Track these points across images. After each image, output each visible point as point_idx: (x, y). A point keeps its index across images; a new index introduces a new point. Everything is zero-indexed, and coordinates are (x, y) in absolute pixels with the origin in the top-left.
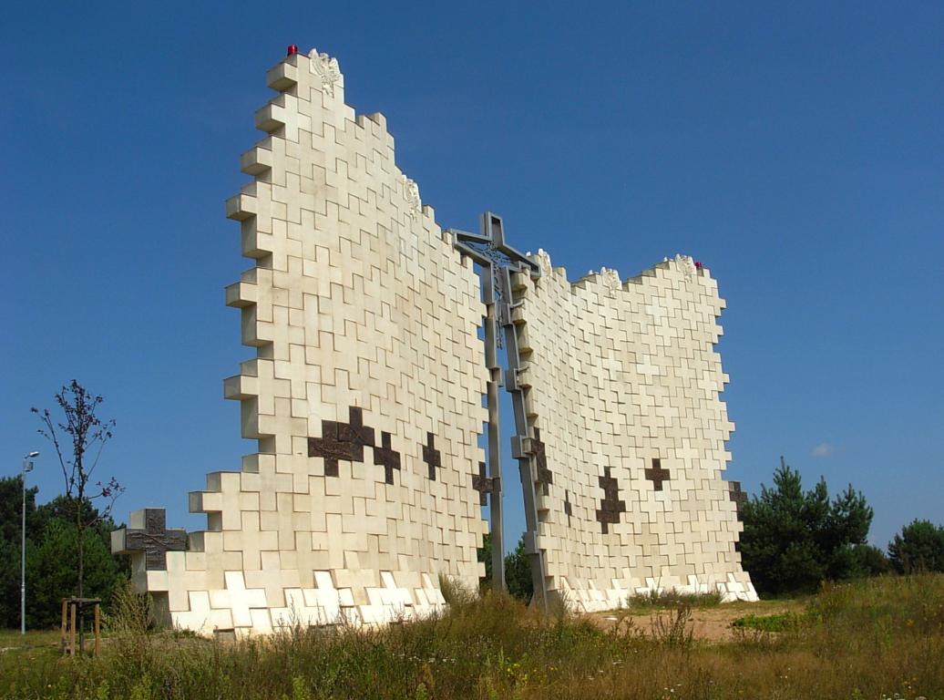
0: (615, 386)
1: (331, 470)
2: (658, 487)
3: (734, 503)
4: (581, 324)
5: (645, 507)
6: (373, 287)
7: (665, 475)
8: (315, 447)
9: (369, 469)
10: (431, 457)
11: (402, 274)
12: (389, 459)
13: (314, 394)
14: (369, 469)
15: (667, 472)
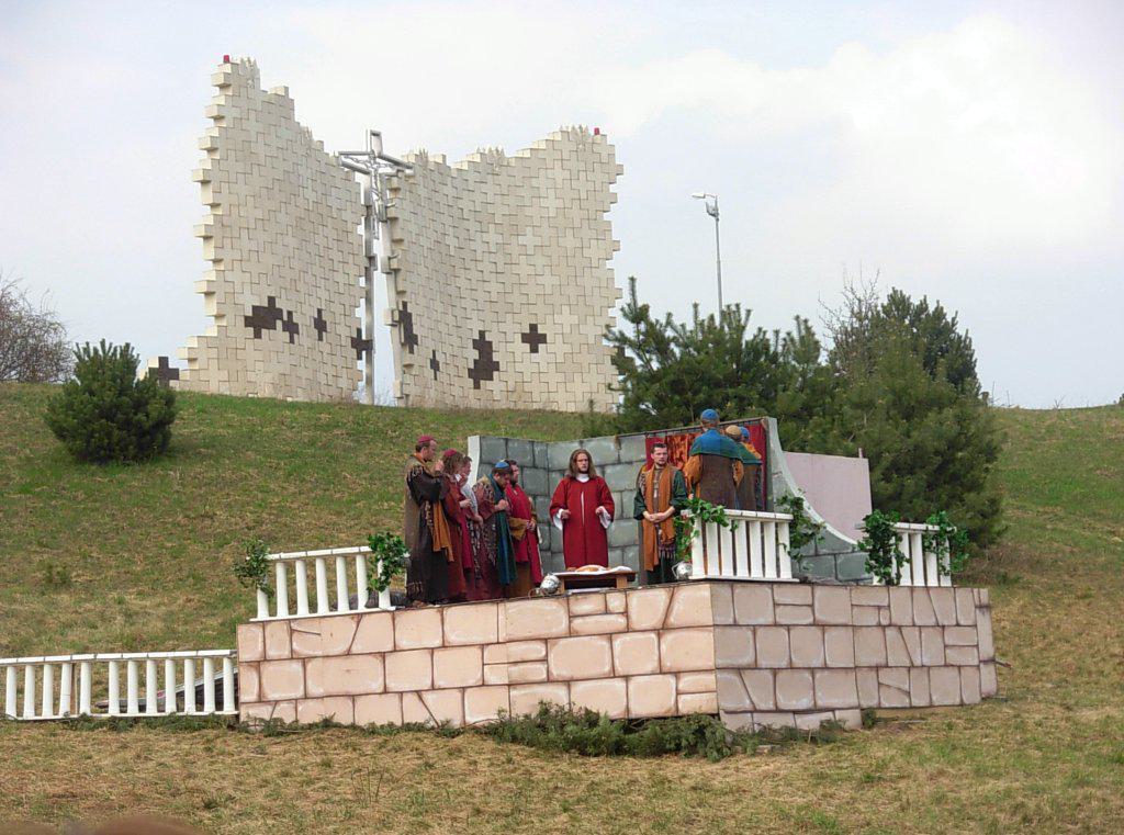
1: (258, 335)
2: (534, 350)
3: (495, 359)
4: (461, 204)
5: (519, 367)
6: (282, 217)
7: (543, 339)
8: (248, 322)
9: (279, 334)
10: (320, 325)
11: (301, 201)
12: (292, 328)
13: (247, 289)
14: (279, 334)
15: (544, 336)
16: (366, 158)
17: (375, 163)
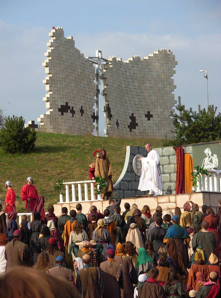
0: (136, 91)
1: (62, 114)
2: (149, 119)
4: (126, 73)
5: (144, 125)
9: (69, 114)
10: (82, 111)
12: (73, 112)
13: (59, 100)
14: (69, 114)
15: (152, 115)
16: (97, 59)
17: (100, 61)
